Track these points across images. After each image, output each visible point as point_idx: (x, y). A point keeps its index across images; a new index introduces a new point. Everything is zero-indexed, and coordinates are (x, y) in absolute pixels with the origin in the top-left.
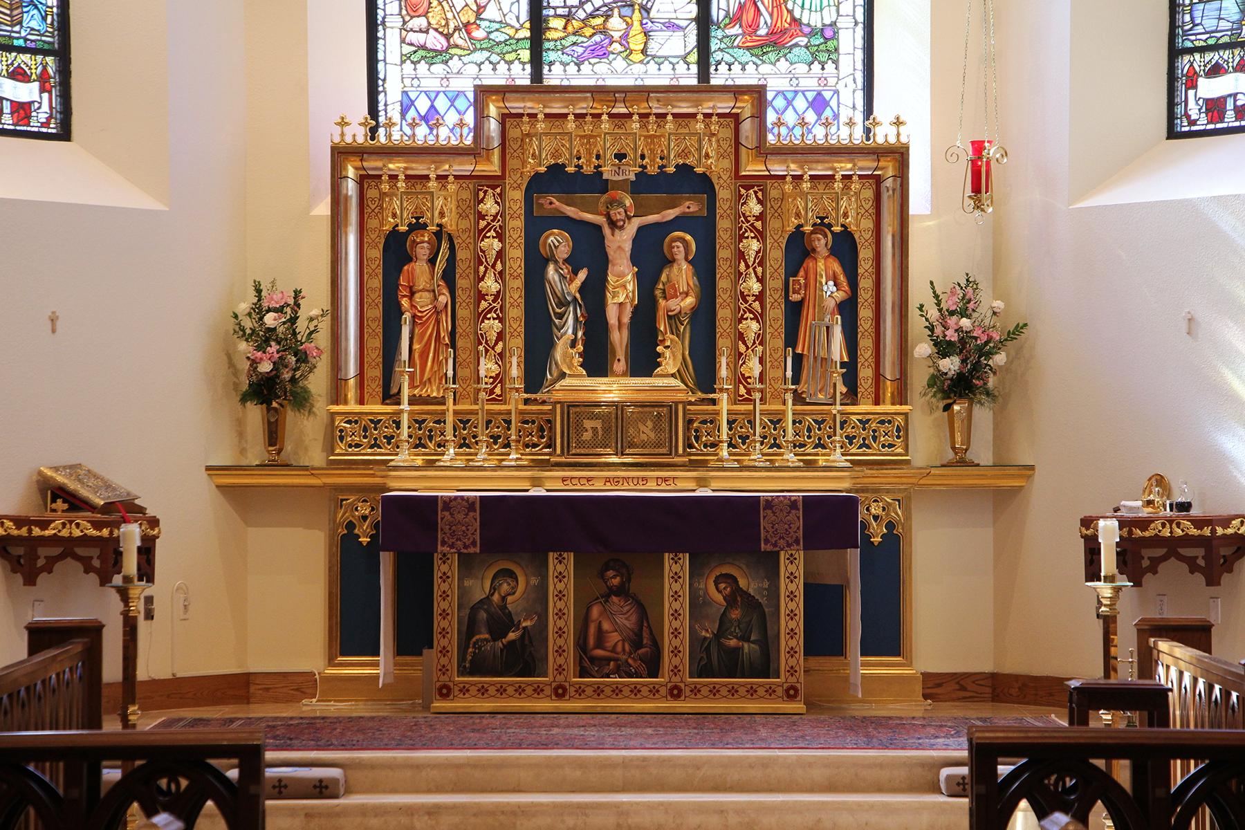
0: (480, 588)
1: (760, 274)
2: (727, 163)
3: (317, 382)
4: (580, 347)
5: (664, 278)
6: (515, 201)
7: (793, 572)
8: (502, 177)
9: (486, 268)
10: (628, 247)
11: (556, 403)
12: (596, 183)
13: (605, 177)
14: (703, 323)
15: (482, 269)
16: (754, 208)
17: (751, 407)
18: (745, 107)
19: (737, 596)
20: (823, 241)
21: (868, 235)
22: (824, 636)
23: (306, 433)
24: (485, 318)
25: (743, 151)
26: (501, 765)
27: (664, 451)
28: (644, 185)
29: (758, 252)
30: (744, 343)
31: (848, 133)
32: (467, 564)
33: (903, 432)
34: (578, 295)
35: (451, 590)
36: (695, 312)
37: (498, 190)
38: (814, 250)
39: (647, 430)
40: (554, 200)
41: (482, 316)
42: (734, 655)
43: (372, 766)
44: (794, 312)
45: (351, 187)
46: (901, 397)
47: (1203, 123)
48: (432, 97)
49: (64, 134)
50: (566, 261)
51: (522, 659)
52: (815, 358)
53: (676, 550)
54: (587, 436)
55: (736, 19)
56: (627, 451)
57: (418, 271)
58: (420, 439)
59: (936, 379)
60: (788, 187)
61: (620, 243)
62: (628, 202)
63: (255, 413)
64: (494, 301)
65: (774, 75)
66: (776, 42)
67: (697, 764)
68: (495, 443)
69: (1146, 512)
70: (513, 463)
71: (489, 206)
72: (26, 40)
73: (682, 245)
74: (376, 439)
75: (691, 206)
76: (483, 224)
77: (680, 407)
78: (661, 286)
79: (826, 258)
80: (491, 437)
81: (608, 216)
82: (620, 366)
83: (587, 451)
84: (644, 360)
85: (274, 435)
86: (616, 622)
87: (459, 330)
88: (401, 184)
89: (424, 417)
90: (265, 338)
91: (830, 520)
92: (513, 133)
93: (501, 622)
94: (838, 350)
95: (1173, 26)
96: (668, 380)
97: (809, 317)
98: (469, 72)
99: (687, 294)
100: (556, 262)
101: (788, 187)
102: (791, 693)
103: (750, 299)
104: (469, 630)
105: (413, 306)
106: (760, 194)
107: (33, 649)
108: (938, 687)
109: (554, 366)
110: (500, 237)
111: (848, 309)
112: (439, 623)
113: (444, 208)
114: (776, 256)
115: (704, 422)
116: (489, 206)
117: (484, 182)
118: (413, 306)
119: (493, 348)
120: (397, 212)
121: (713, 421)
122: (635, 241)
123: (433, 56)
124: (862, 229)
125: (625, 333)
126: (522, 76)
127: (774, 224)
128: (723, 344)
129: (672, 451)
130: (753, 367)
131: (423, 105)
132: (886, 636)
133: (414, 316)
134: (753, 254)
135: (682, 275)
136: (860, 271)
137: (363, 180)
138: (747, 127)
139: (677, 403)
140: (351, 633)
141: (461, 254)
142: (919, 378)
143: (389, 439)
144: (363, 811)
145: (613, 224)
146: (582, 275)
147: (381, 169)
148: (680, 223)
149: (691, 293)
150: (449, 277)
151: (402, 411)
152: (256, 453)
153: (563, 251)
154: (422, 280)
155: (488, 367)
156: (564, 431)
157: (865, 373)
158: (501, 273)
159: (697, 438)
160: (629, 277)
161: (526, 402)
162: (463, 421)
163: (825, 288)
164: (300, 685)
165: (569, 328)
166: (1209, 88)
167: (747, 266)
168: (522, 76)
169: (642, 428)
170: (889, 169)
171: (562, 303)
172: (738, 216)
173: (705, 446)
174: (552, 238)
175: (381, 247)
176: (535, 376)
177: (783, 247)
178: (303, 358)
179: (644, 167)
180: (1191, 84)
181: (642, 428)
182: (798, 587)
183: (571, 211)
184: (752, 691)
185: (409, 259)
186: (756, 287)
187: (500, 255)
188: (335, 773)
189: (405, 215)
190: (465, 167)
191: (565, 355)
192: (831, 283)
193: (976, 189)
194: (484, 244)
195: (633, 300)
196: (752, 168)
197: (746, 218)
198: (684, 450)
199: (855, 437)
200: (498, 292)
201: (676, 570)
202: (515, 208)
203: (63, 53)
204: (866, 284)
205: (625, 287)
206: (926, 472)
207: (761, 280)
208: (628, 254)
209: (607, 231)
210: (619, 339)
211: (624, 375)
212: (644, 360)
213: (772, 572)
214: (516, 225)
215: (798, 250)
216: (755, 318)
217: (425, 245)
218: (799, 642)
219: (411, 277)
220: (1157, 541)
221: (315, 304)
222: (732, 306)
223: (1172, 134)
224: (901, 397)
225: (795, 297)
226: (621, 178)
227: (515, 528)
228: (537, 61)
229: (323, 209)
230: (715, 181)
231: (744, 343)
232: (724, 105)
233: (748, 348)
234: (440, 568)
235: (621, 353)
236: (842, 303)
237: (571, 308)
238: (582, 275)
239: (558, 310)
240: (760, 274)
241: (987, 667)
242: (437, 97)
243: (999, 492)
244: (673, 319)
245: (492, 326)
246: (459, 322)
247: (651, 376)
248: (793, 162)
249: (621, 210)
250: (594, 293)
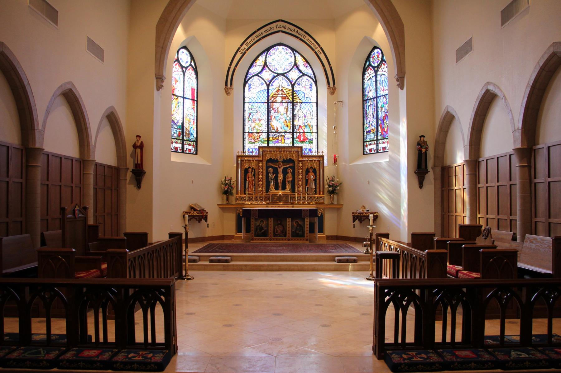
0: (258, 223)
3: (234, 191)
7: (307, 221)
12: (276, 161)
16: (301, 165)
18: (299, 150)
19: (298, 225)
22: (312, 230)
23: (233, 199)
26: (259, 256)
28: (285, 161)
31: (316, 154)
32: (256, 220)
33: (324, 199)
35: (253, 223)
41: (259, 181)
42: (298, 233)
43: (236, 256)
44: (307, 181)
45: (239, 162)
46: (323, 194)
47: (369, 152)
48: (252, 149)
49: (196, 154)
51: (264, 234)
53: (289, 217)
55: (298, 138)
57: (250, 174)
59: (329, 191)
61: (280, 170)
63: (225, 196)
65: (305, 146)
66: (303, 141)
67: (293, 256)
69: (362, 212)
71: (260, 165)
72: (372, 271)
73: (290, 170)
75: (291, 165)
84: (284, 188)
85: (227, 199)
86: (279, 229)
90: (226, 184)
91: (313, 213)
92: (264, 154)
93: (261, 228)
94: (314, 187)
95: (363, 138)
96: (288, 191)
97: (309, 181)
98: (257, 145)
102: (307, 240)
104: (256, 230)
107: (169, 238)
108: (328, 238)
111: (315, 180)
112: (251, 229)
113: (253, 165)
114: (304, 172)
116: (260, 165)
120: (246, 166)
121: (295, 197)
122: (283, 170)
123: (254, 143)
124: (317, 168)
126: (266, 145)
128: (296, 186)
129: (288, 202)
130: (301, 189)
131: (251, 150)
132: (321, 230)
135: (290, 175)
137: (241, 161)
138: (300, 153)
140: (239, 230)
142: (326, 191)
144: (233, 265)
148: (289, 167)
150: (254, 175)
152: (225, 202)
153: (272, 171)
154: (250, 176)
155: (260, 189)
156: (274, 199)
157: (318, 190)
162: (256, 197)
164: (231, 237)
165: (272, 183)
166: (369, 147)
168: (266, 145)
170: (321, 159)
172: (298, 166)
178: (232, 187)
180: (367, 146)
182: (308, 223)
184: (301, 240)
188: (229, 258)
190: (257, 159)
193: (335, 162)
196: (301, 159)
201: (289, 220)
203: (196, 142)
204: (318, 176)
206: (327, 205)
210: (280, 185)
212: (284, 188)
213: (304, 220)
214: (265, 168)
215: (307, 171)
218: (308, 232)
220: (364, 216)
221: (234, 179)
223: (364, 154)
224: (323, 194)
227: (263, 214)
228: (268, 144)
229: (235, 165)
232: (296, 150)
234: (252, 220)
241: (336, 235)
242: (252, 148)
243: (338, 209)
244: (289, 182)
245: (261, 183)
250: (276, 178)
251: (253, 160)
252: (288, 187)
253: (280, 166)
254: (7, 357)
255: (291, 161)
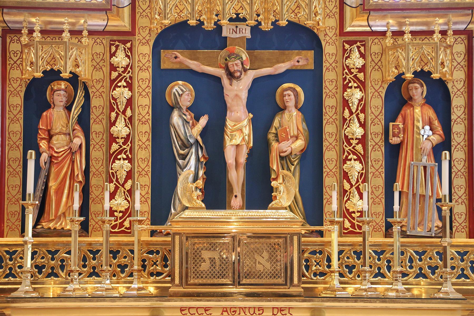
1: (362, 120)
2: (333, 22)
4: (200, 183)
5: (276, 123)
6: (144, 55)
8: (132, 33)
9: (118, 115)
10: (244, 95)
11: (175, 234)
12: (214, 39)
13: (224, 34)
14: (311, 163)
15: (113, 115)
17: (361, 239)
20: (420, 90)
21: (460, 85)
24: (116, 158)
25: (348, 10)
27: (281, 281)
28: (265, 39)
29: (360, 101)
30: (349, 181)
34: (199, 139)
36: (304, 154)
37: (129, 45)
38: (411, 98)
39: (263, 261)
40: (179, 55)
41: (113, 157)
44: (393, 153)
50: (189, 109)
52: (414, 195)
54: (205, 266)
56: (244, 281)
57: (57, 118)
58: (463, 270)
60: (389, 41)
61: (237, 93)
62: (245, 56)
64: (124, 143)
68: (123, 272)
70: (135, 292)
71: (120, 59)
73: (292, 94)
74: (11, 269)
76: (115, 74)
77: (295, 238)
78: (273, 131)
79: (422, 106)
80: (119, 266)
81: (227, 69)
82: (237, 201)
83: (205, 281)
87: (92, 169)
88: (37, 35)
89: (57, 248)
96: (283, 211)
97: (406, 158)
99: (297, 138)
100: (180, 109)
101: (389, 41)
103: (354, 142)
105: (50, 148)
106: (362, 49)
109: (177, 201)
110: (130, 86)
114: (377, 104)
115: (314, 253)
117: (115, 38)
118: (50, 148)
119: (123, 186)
125: (242, 172)
127: (376, 75)
129: (289, 281)
133: (51, 157)
134: (356, 102)
135: (292, 121)
136: (453, 117)
139: (292, 235)
141: (95, 102)
143: (433, 269)
145: (231, 75)
146: (204, 121)
147: (21, 23)
149: (301, 136)
150: (84, 121)
151: (26, 242)
158: (130, 119)
159: (307, 267)
160: (245, 122)
161: (153, 233)
163: (422, 132)
167: (351, 113)
169: (259, 258)
171: (185, 145)
173: (315, 275)
174: (177, 88)
175: (22, 94)
176: (161, 209)
177: (383, 95)
179: (260, 24)
181: (259, 258)
183: (194, 65)
185: (48, 106)
186: (359, 132)
187: (130, 102)
189: (40, 62)
190: (97, 22)
191: (185, 189)
192: (427, 128)
194: (116, 93)
195: (248, 143)
196: (356, 25)
197: (349, 70)
198: (299, 280)
199: (44, 267)
200: (128, 136)
202: (144, 61)
205: (241, 130)
207: (363, 125)
208: (245, 101)
209: (225, 81)
210: (236, 177)
211: (241, 208)
212: (259, 195)
214: (144, 77)
216: (359, 159)
217: (62, 92)
219: (50, 122)
222: (337, 148)
225: (394, 140)
226: (238, 36)
230: (321, 37)
231: (349, 181)
233: (352, 186)
235: (238, 189)
236: (437, 145)
237: (193, 150)
238: (204, 121)
239: (182, 152)
240: (362, 120)
244: (285, 159)
245: (121, 166)
246: (93, 163)
247: (266, 209)
248: (392, 18)
249: (238, 62)
250: (214, 137)
251: (76, 33)
252: (286, 189)
253: (235, 66)
254: (177, 166)
255: (301, 36)
